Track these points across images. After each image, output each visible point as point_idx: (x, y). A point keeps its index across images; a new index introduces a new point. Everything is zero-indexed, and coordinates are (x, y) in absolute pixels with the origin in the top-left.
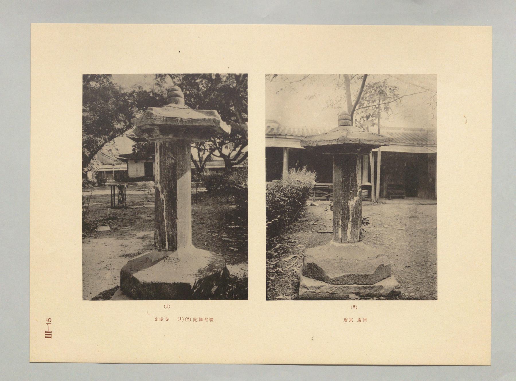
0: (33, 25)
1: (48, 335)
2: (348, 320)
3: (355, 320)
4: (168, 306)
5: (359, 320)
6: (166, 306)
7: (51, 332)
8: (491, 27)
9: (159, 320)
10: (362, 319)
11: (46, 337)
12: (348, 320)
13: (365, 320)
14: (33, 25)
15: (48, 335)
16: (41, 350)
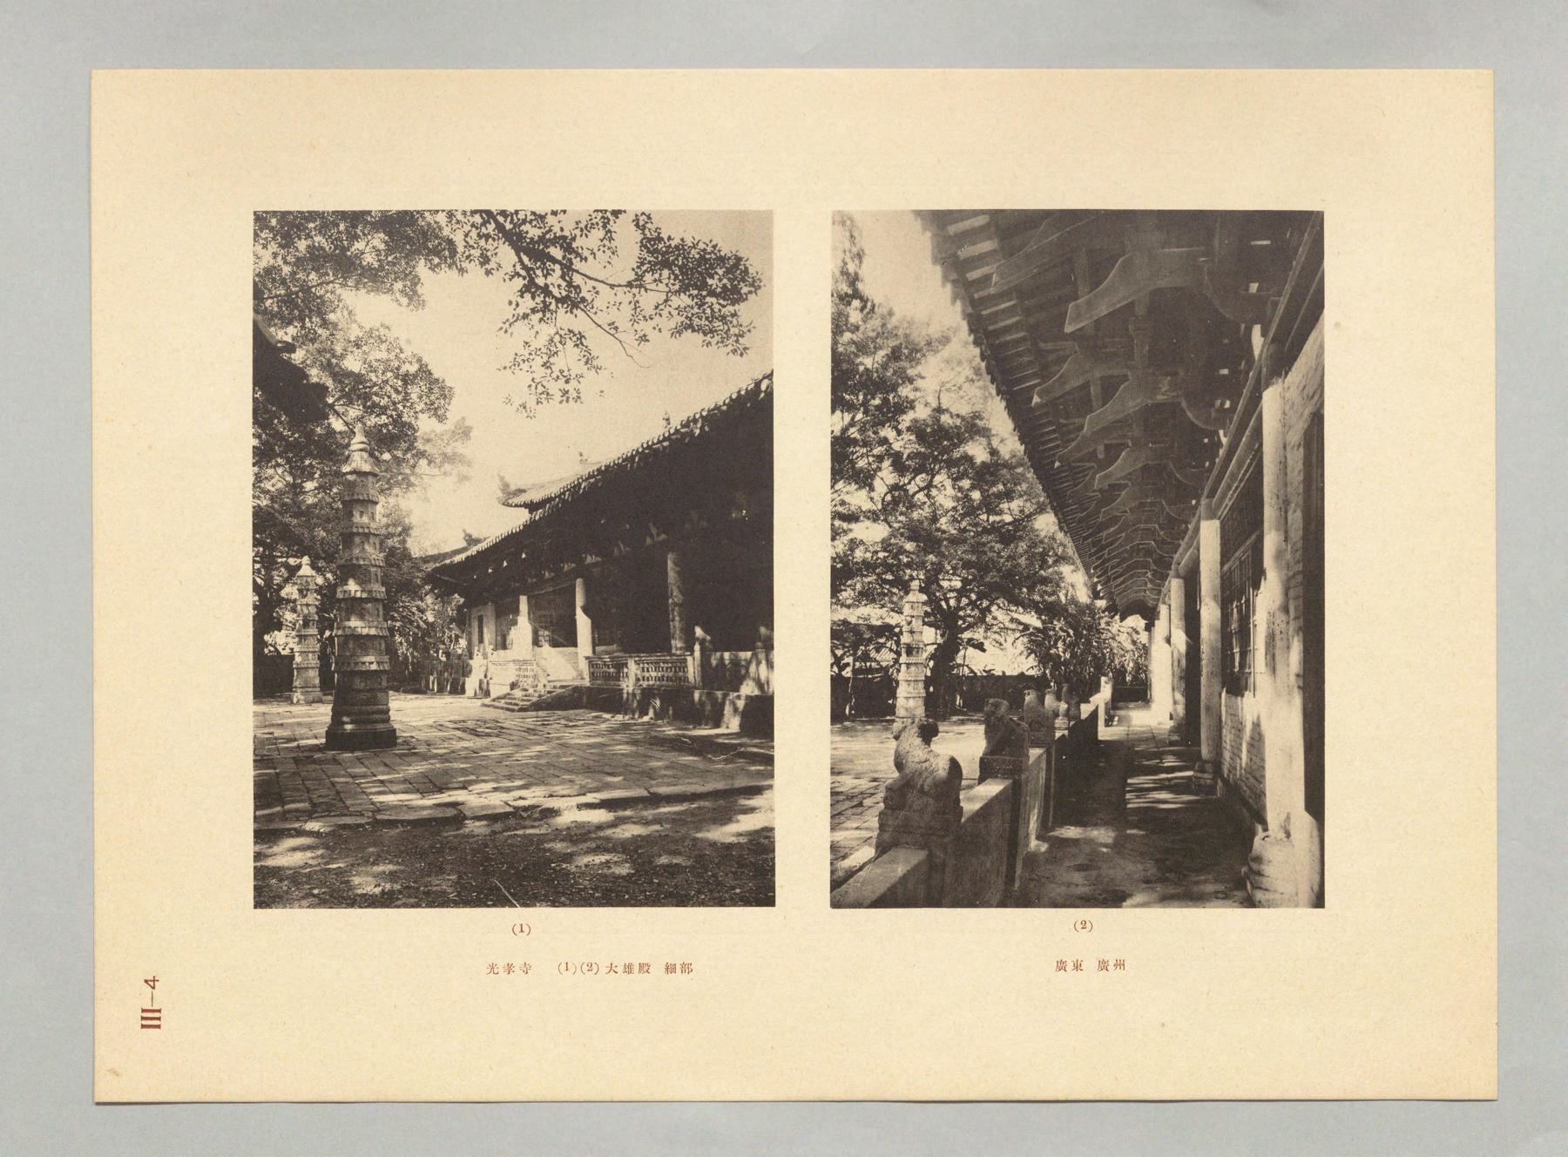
1: (151, 1019)
2: (1070, 966)
3: (1090, 965)
4: (526, 929)
5: (670, 969)
6: (517, 929)
8: (1487, 74)
9: (501, 971)
11: (143, 1026)
12: (1070, 966)
13: (1120, 964)
15: (151, 1019)
16: (129, 1066)
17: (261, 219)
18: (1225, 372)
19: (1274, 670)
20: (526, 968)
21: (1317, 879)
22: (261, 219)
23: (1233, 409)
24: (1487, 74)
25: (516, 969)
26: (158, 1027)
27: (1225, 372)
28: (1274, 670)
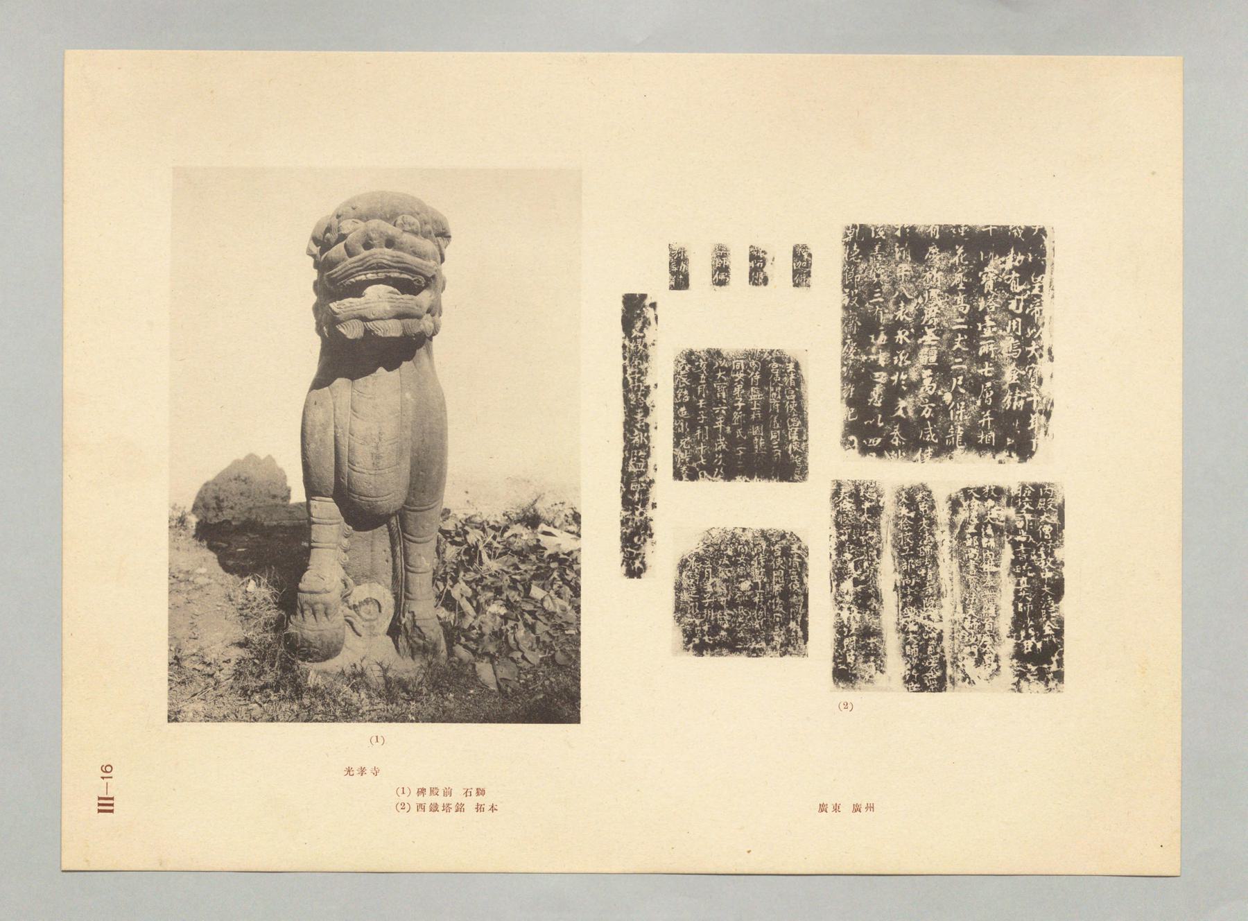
0: (70, 54)
1: (106, 805)
2: (830, 808)
5: (857, 809)
6: (400, 791)
8: (1176, 62)
10: (864, 806)
11: (100, 811)
12: (830, 808)
13: (870, 807)
14: (70, 54)
15: (106, 805)
16: (86, 841)
17: (796, 285)
19: (359, 635)
20: (376, 772)
22: (796, 285)
24: (1176, 62)
26: (112, 811)
28: (359, 635)
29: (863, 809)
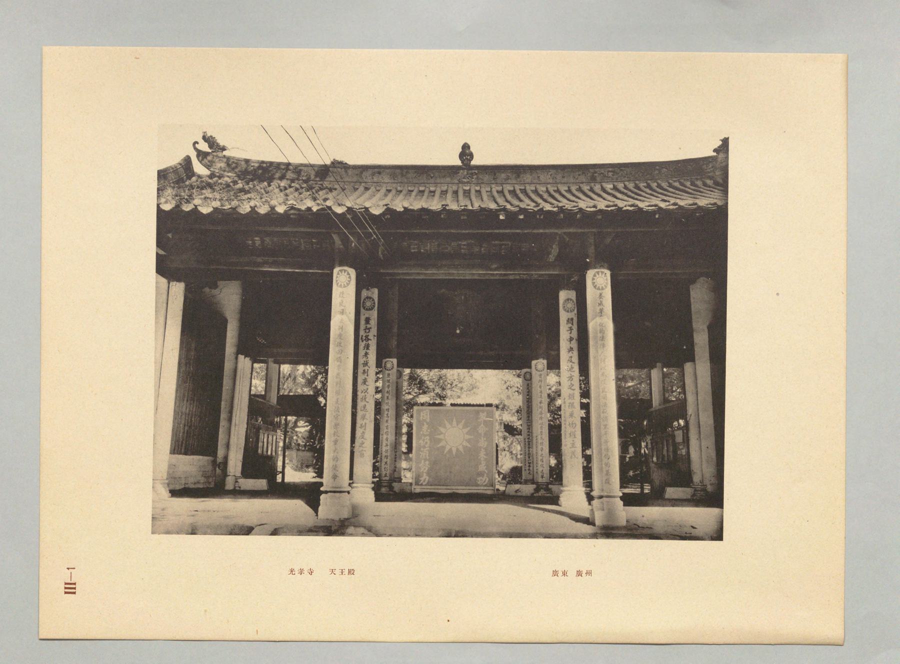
0: (46, 49)
1: (70, 588)
2: (560, 574)
3: (572, 573)
5: (579, 573)
7: (75, 584)
9: (296, 572)
11: (66, 593)
12: (560, 574)
13: (589, 573)
15: (70, 588)
16: (59, 616)
18: (458, 331)
21: (532, 531)
23: (687, 423)
25: (306, 572)
26: (74, 593)
27: (458, 331)
29: (584, 575)
